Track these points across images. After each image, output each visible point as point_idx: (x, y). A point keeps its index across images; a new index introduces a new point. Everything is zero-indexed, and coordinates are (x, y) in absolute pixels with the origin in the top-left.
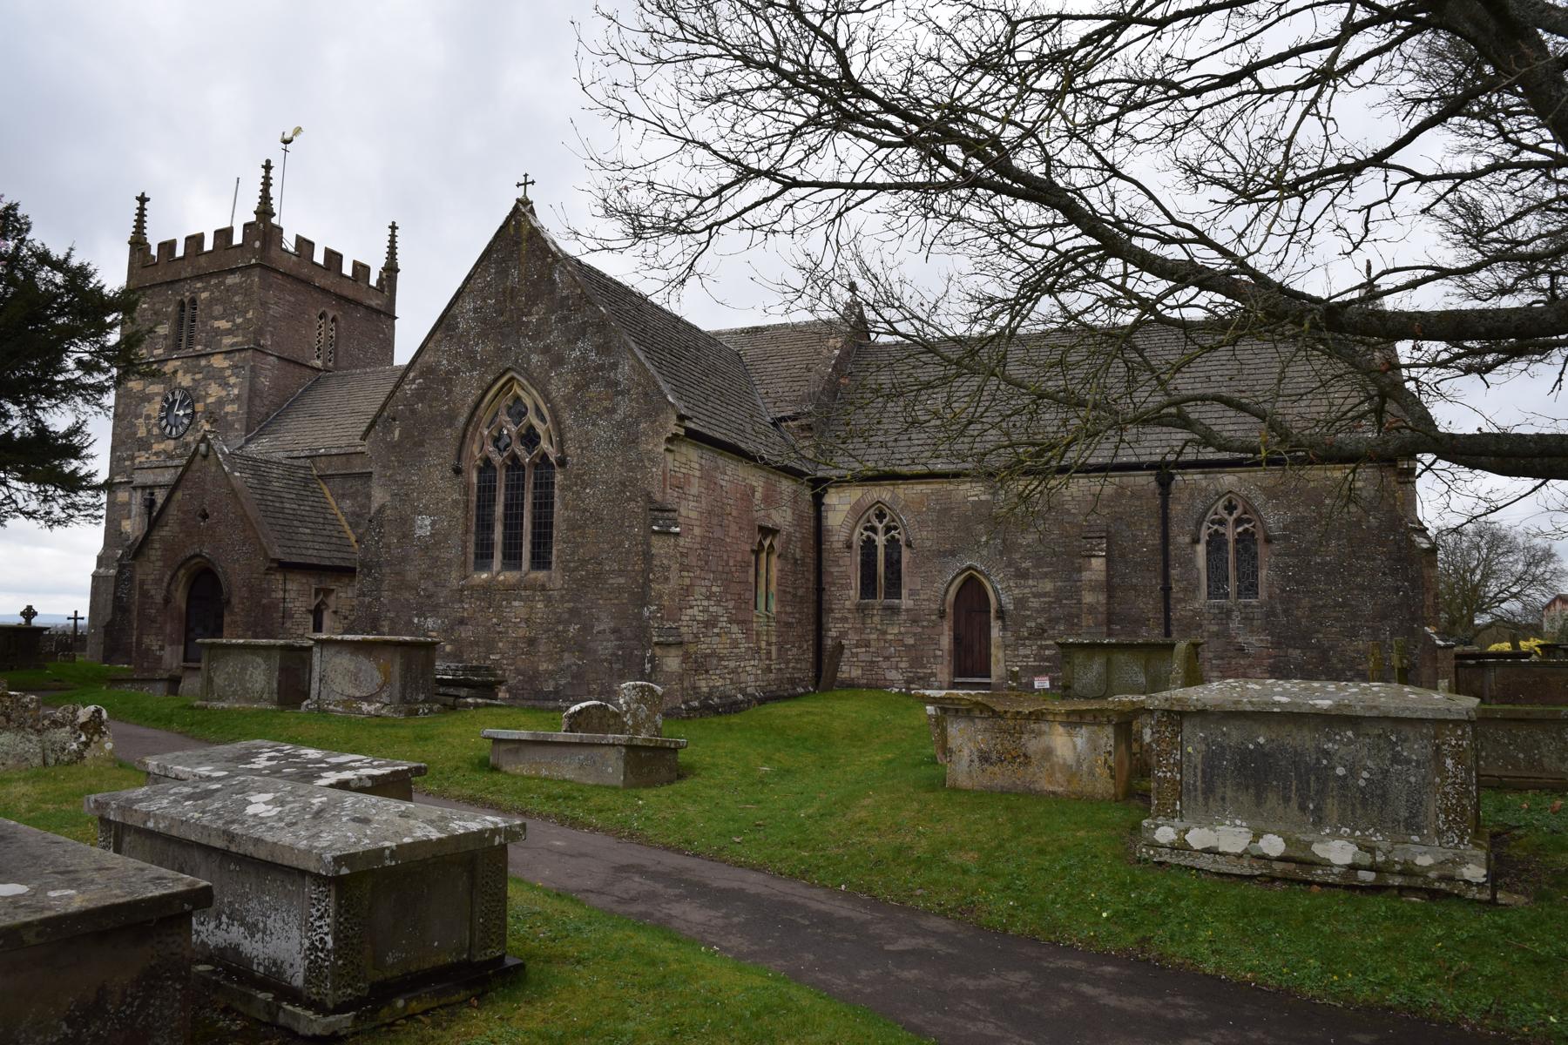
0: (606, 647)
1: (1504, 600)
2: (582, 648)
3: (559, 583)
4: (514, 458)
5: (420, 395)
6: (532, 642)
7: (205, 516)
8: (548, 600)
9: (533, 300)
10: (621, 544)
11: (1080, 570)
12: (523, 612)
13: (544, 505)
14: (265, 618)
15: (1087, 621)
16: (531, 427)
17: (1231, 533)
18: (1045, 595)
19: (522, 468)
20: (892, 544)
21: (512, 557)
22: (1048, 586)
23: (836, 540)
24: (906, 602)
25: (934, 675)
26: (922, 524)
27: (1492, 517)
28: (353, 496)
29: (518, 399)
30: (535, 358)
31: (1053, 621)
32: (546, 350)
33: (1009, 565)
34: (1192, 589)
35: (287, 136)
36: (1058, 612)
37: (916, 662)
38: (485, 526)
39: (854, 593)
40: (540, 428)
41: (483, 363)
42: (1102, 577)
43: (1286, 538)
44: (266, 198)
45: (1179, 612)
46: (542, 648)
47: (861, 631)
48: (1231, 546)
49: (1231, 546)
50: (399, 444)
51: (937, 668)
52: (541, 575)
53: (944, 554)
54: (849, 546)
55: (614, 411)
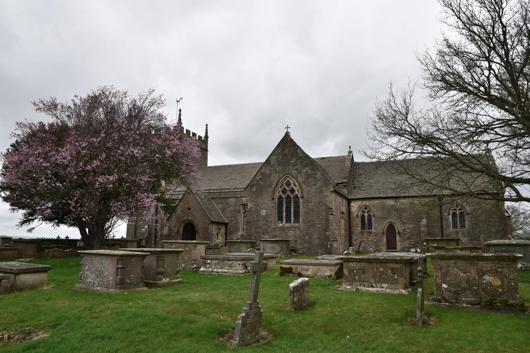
0: (316, 242)
1: (517, 230)
2: (310, 242)
3: (303, 227)
4: (288, 196)
5: (261, 179)
6: (296, 241)
7: (189, 209)
8: (300, 231)
9: (292, 157)
10: (319, 217)
11: (420, 222)
12: (293, 234)
13: (297, 207)
14: (207, 236)
15: (422, 235)
16: (292, 188)
17: (458, 213)
18: (411, 228)
19: (291, 198)
20: (369, 216)
21: (288, 220)
22: (411, 226)
23: (354, 215)
24: (374, 230)
25: (381, 249)
26: (377, 211)
27: (152, 96)
28: (222, 203)
29: (288, 181)
30: (293, 171)
31: (413, 235)
32: (297, 169)
33: (401, 221)
34: (449, 226)
35: (178, 100)
36: (414, 232)
37: (377, 246)
38: (280, 212)
39: (359, 228)
40: (295, 188)
41: (279, 172)
42: (426, 224)
43: (472, 213)
44: (180, 119)
45: (445, 232)
46: (299, 242)
47: (362, 238)
48: (458, 216)
49: (458, 216)
50: (255, 191)
51: (383, 248)
52: (297, 224)
53: (384, 218)
54: (358, 216)
55: (316, 185)
